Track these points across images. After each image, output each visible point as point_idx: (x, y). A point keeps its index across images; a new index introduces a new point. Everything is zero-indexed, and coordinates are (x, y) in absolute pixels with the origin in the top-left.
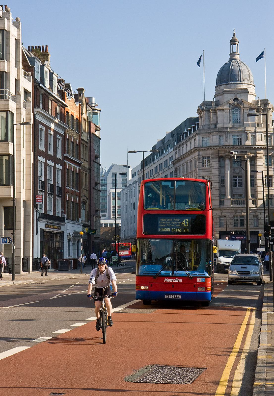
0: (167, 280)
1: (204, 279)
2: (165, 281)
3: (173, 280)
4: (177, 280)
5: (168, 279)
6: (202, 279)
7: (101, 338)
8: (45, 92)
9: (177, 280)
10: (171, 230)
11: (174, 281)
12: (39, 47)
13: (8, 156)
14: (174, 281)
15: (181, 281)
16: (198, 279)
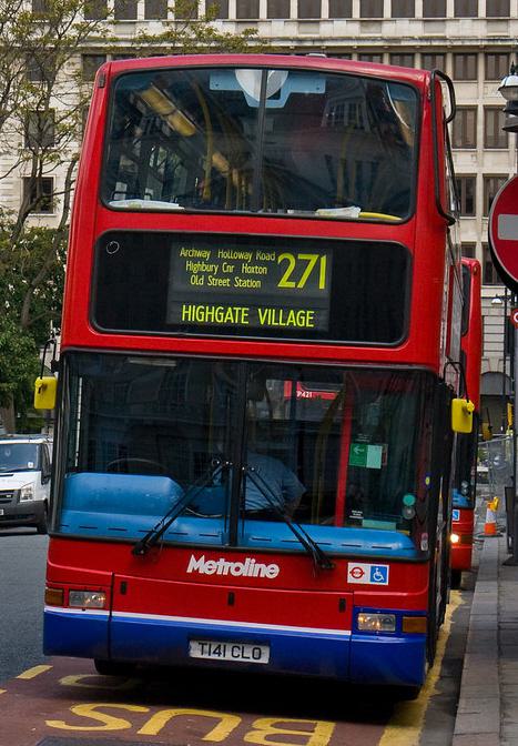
0: (198, 565)
1: (383, 571)
2: (189, 570)
3: (233, 565)
4: (250, 568)
5: (206, 561)
6: (373, 570)
7: (465, 60)
8: (369, 81)
9: (250, 568)
10: (253, 316)
11: (237, 569)
12: (47, 592)
13: (489, 113)
14: (237, 569)
15: (271, 571)
16: (351, 566)
